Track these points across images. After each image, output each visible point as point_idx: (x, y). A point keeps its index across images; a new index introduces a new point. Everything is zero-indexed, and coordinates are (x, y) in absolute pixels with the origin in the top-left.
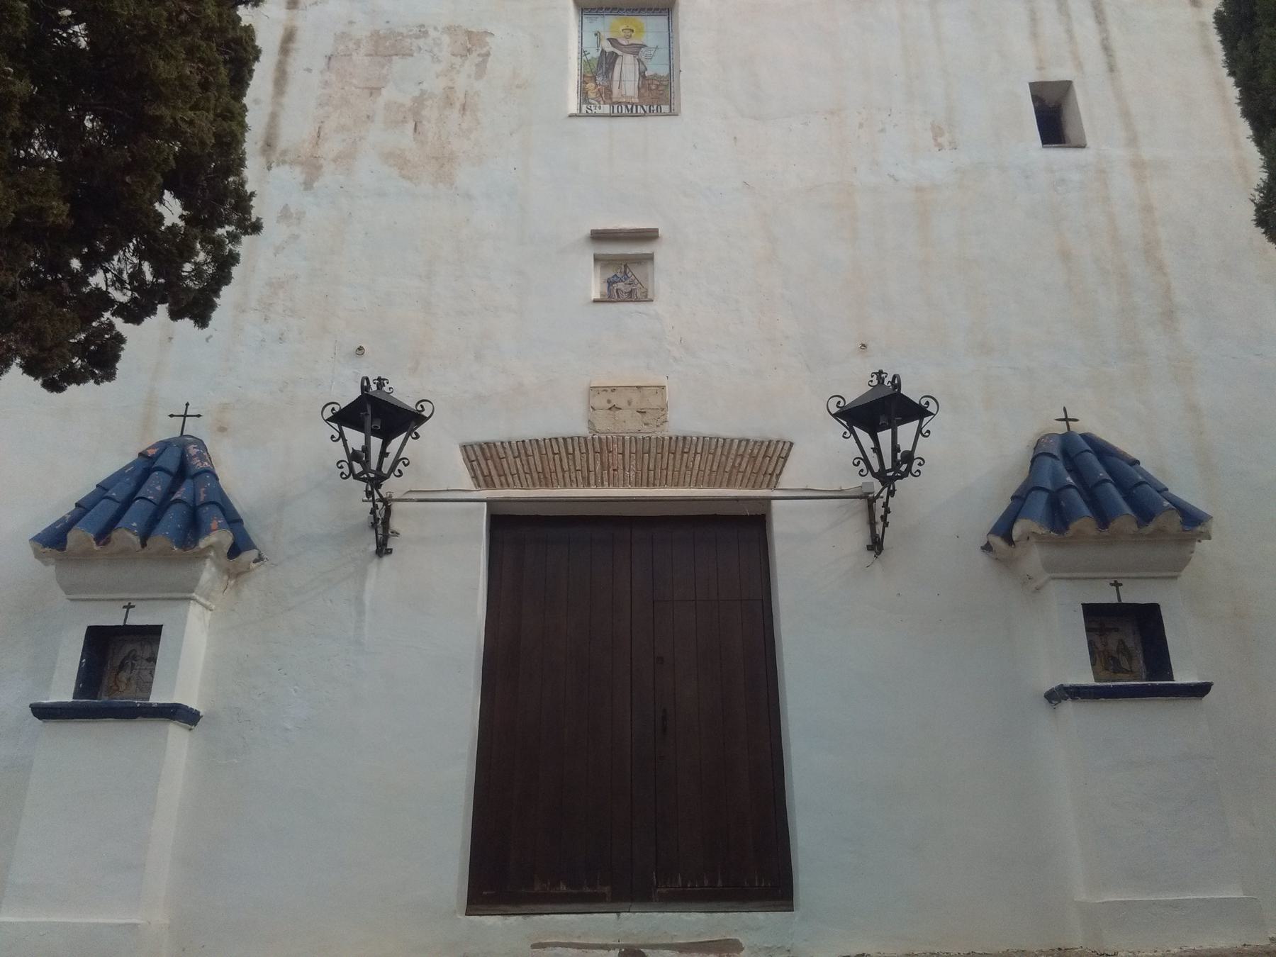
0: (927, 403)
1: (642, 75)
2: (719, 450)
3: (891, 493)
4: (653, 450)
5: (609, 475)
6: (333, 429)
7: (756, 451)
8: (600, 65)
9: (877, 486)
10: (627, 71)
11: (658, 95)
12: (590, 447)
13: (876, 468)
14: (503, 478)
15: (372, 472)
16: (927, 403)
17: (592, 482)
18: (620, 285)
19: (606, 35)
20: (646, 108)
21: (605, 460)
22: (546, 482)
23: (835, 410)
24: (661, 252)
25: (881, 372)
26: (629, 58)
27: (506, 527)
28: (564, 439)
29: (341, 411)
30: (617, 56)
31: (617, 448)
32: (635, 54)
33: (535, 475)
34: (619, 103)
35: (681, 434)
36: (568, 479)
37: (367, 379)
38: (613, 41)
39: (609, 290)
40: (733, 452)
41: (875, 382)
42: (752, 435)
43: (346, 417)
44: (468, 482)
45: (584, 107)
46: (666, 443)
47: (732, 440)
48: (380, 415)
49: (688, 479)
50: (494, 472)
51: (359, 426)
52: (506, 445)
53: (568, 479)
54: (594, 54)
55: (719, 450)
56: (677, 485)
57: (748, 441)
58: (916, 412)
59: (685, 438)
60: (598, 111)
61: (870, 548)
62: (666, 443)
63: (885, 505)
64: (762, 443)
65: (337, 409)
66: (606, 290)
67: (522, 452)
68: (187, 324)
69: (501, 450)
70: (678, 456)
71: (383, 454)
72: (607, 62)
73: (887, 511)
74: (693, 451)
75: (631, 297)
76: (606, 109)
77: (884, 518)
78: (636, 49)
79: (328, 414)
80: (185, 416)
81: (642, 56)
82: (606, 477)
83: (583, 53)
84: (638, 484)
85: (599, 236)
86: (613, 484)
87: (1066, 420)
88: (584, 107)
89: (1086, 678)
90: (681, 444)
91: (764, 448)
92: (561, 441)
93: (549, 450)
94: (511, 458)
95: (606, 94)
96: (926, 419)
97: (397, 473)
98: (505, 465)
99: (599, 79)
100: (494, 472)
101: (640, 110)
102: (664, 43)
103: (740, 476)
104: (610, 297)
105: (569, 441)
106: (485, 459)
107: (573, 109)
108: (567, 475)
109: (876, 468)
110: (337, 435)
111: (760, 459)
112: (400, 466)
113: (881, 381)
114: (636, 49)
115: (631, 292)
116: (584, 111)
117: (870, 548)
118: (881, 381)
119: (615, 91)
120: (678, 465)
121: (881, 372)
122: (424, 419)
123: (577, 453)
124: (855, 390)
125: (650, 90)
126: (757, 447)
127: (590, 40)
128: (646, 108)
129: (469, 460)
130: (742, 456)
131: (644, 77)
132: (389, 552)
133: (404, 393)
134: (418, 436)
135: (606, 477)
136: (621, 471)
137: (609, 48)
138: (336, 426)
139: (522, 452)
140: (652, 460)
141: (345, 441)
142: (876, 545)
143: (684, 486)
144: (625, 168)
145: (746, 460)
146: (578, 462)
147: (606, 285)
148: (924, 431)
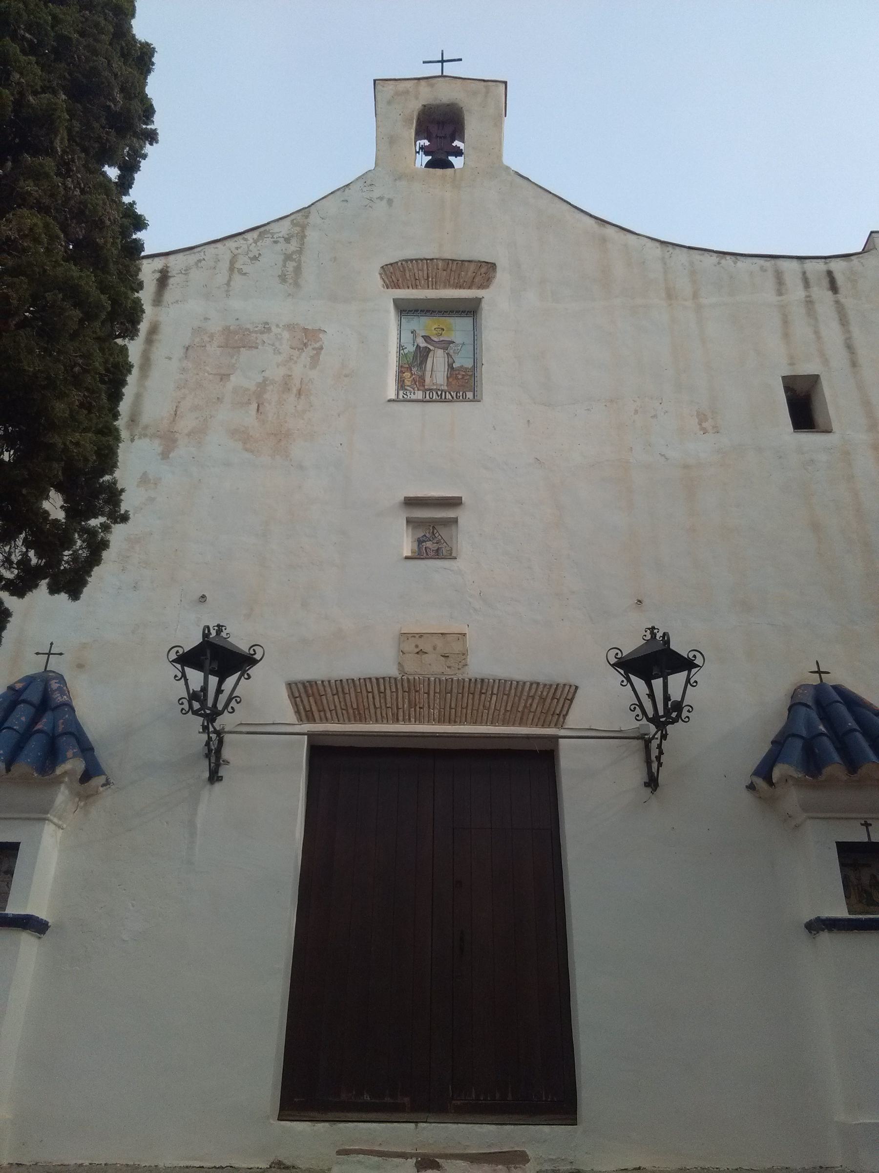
0: (695, 656)
1: (451, 366)
2: (513, 691)
3: (664, 737)
4: (455, 691)
7: (545, 694)
10: (437, 364)
11: (464, 384)
12: (399, 686)
13: (650, 714)
16: (695, 656)
17: (401, 718)
20: (454, 394)
23: (613, 661)
25: (653, 628)
26: (440, 352)
27: (328, 761)
28: (377, 679)
30: (430, 350)
31: (423, 688)
32: (445, 349)
33: (351, 711)
34: (431, 390)
35: (479, 676)
38: (426, 338)
41: (649, 637)
46: (467, 684)
47: (525, 683)
48: (217, 657)
49: (485, 718)
51: (198, 666)
52: (326, 683)
54: (411, 348)
55: (513, 691)
56: (475, 723)
57: (538, 684)
58: (686, 664)
59: (482, 680)
60: (413, 397)
61: (647, 785)
62: (467, 684)
63: (659, 746)
64: (551, 686)
67: (340, 690)
69: (321, 688)
70: (477, 697)
71: (219, 691)
72: (422, 355)
73: (661, 753)
75: (438, 555)
76: (419, 395)
77: (658, 758)
78: (446, 345)
79: (173, 656)
80: (49, 654)
82: (413, 713)
83: (401, 347)
84: (441, 721)
85: (411, 502)
86: (419, 720)
87: (819, 672)
88: (401, 393)
92: (374, 681)
93: (364, 688)
95: (420, 383)
96: (694, 671)
97: (230, 709)
98: (325, 702)
99: (414, 370)
100: (314, 708)
101: (448, 396)
104: (420, 554)
105: (381, 681)
106: (307, 696)
109: (650, 714)
111: (549, 700)
112: (233, 703)
113: (653, 635)
117: (647, 785)
119: (428, 380)
121: (653, 628)
123: (388, 692)
125: (457, 378)
127: (407, 337)
128: (454, 394)
129: (293, 697)
130: (533, 698)
131: (452, 368)
133: (239, 638)
134: (249, 677)
135: (413, 713)
136: (426, 709)
137: (423, 344)
138: (179, 666)
139: (340, 690)
141: (186, 680)
144: (436, 446)
147: (416, 544)
148: (692, 681)
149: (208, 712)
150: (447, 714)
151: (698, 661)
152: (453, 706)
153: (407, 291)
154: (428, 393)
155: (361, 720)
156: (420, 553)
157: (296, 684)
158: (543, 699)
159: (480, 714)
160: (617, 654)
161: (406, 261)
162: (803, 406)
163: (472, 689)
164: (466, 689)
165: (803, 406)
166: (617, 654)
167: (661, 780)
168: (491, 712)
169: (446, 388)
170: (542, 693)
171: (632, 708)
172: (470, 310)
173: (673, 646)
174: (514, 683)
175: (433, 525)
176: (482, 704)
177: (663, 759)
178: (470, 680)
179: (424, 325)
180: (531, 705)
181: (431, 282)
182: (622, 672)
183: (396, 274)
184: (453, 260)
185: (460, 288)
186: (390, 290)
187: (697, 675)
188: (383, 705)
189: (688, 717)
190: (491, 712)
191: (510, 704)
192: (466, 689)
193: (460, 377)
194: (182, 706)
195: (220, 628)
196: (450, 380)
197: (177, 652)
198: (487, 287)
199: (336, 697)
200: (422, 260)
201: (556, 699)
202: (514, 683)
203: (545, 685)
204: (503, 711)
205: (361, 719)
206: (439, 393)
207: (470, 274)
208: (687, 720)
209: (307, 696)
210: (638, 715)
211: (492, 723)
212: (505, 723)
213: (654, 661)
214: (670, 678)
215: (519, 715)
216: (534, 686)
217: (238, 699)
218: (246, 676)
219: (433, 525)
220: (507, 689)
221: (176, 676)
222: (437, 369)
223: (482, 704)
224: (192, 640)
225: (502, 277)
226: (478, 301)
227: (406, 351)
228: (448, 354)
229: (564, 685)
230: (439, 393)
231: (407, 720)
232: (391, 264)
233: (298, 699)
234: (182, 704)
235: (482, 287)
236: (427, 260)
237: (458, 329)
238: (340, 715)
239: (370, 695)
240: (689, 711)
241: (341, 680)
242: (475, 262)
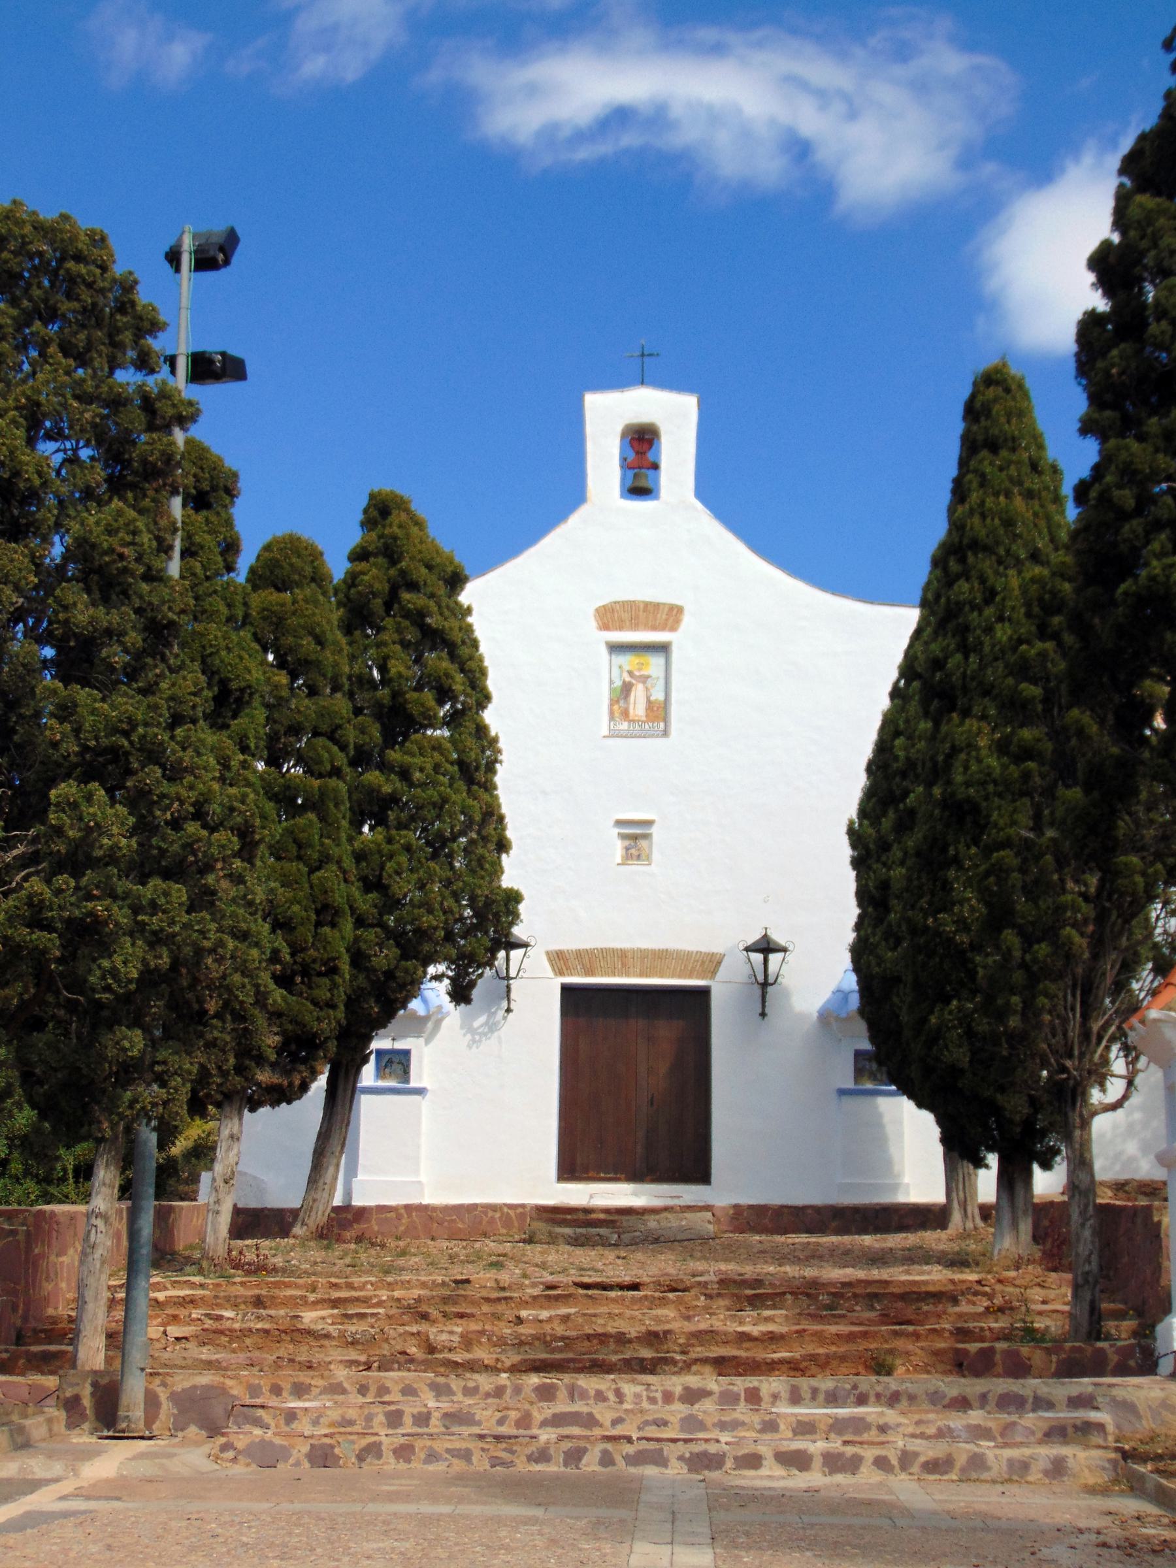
5: (626, 971)
10: (638, 697)
18: (633, 851)
19: (626, 668)
22: (590, 972)
24: (654, 830)
26: (640, 687)
27: (576, 1000)
32: (644, 683)
38: (630, 673)
42: (703, 949)
44: (550, 973)
54: (618, 683)
56: (662, 977)
72: (627, 689)
83: (611, 682)
84: (641, 975)
85: (620, 823)
86: (628, 975)
89: (850, 1084)
95: (625, 714)
102: (662, 675)
106: (559, 960)
107: (606, 733)
114: (645, 679)
119: (631, 711)
124: (753, 937)
127: (616, 672)
129: (550, 960)
137: (628, 679)
142: (763, 1014)
175: (635, 838)
179: (628, 661)
181: (635, 626)
183: (609, 616)
201: (711, 964)
209: (559, 960)
212: (680, 977)
213: (766, 947)
219: (635, 837)
222: (638, 704)
231: (620, 975)
235: (673, 629)
237: (654, 665)
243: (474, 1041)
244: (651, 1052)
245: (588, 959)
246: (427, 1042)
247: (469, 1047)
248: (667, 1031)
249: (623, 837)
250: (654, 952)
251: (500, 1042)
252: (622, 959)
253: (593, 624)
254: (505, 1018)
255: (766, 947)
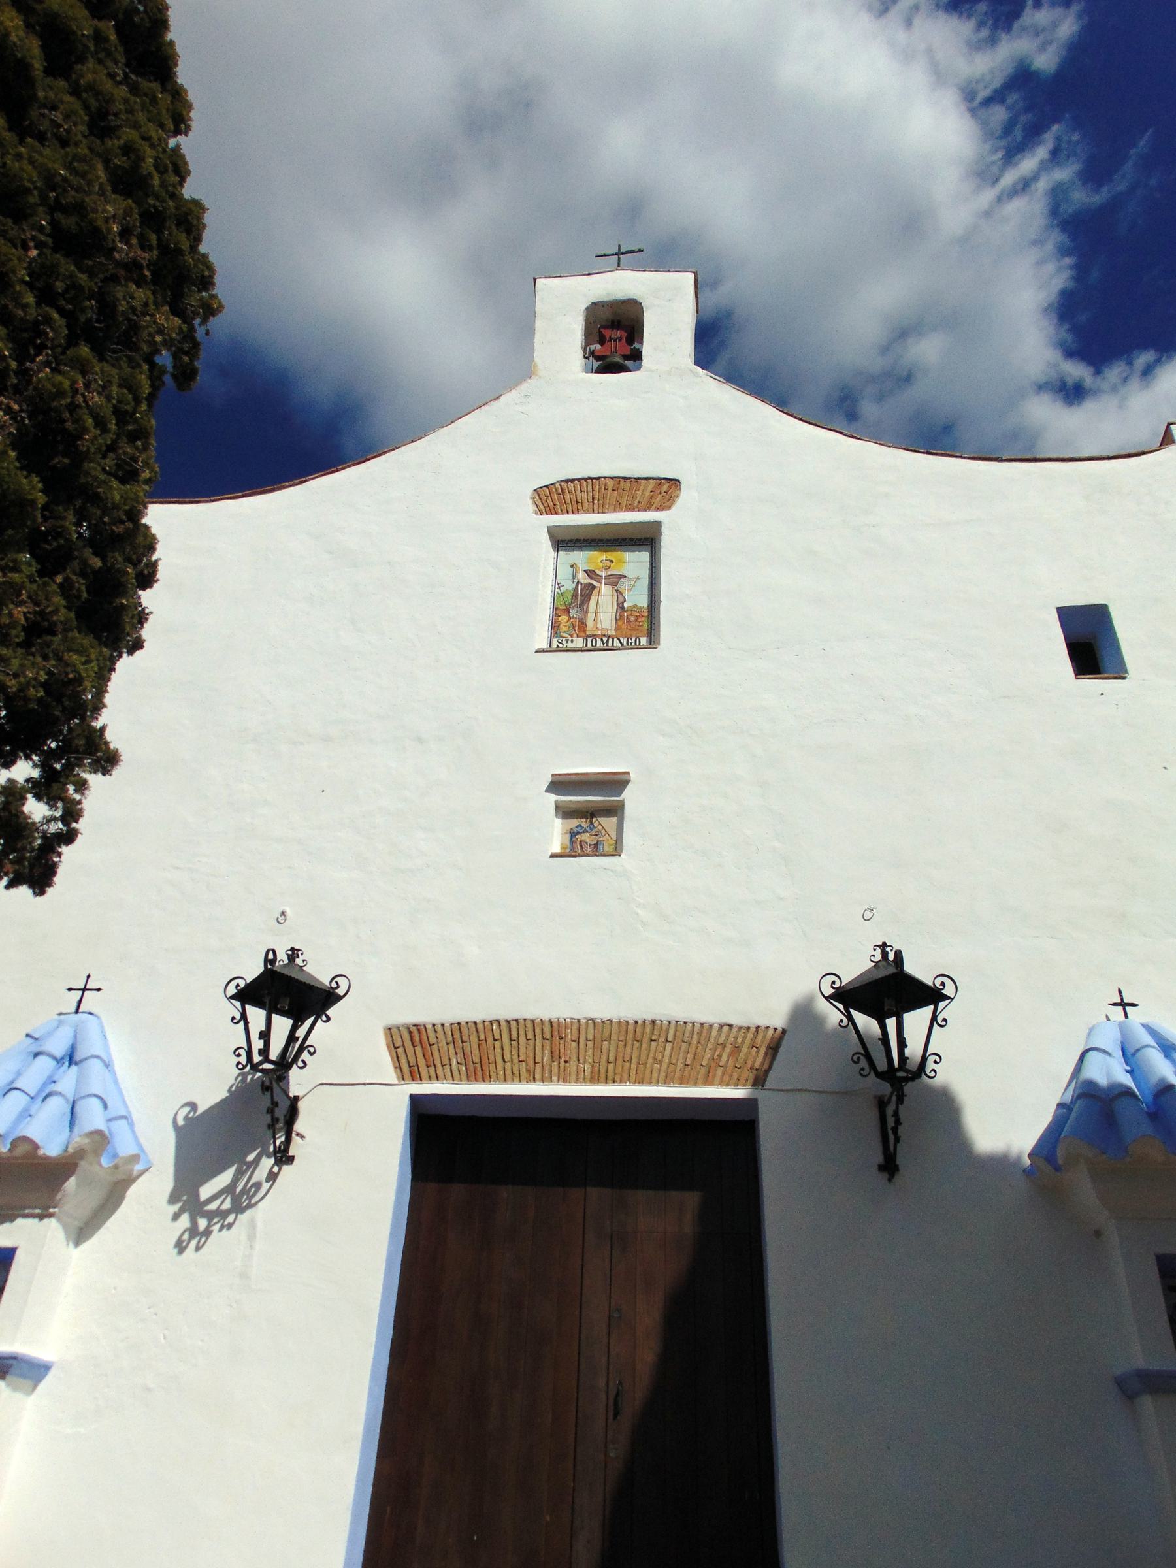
0: (943, 984)
1: (620, 606)
2: (695, 1037)
3: (901, 1099)
4: (614, 1037)
6: (234, 1008)
7: (739, 1040)
8: (575, 596)
9: (886, 1088)
11: (642, 626)
12: (538, 1031)
13: (882, 1065)
14: (432, 1069)
15: (272, 1062)
16: (943, 984)
17: (538, 1076)
18: (586, 837)
19: (582, 567)
20: (624, 641)
21: (555, 1049)
23: (828, 991)
25: (884, 945)
26: (605, 590)
27: (444, 1142)
28: (508, 1022)
29: (248, 986)
30: (594, 587)
31: (570, 1034)
32: (613, 585)
33: (471, 1067)
34: (593, 636)
35: (649, 1017)
36: (508, 1072)
37: (274, 952)
38: (590, 573)
39: (572, 842)
40: (712, 1040)
41: (878, 957)
42: (735, 1021)
43: (247, 995)
45: (555, 641)
46: (631, 1028)
47: (711, 1026)
48: (287, 992)
49: (655, 1075)
50: (422, 1062)
51: (259, 1004)
52: (439, 1028)
53: (508, 1072)
54: (569, 586)
55: (695, 1037)
56: (641, 1082)
57: (731, 1026)
58: (931, 996)
59: (653, 1022)
60: (570, 645)
61: (881, 1168)
62: (631, 1028)
63: (896, 1114)
64: (749, 1028)
65: (242, 984)
66: (568, 843)
67: (457, 1036)
68: (24, 891)
69: (431, 1034)
70: (645, 1045)
71: (292, 1038)
72: (584, 595)
73: (898, 1122)
74: (663, 1039)
75: (596, 850)
76: (579, 643)
77: (895, 1130)
78: (615, 580)
79: (232, 990)
80: (84, 990)
81: (620, 587)
82: (555, 1070)
84: (594, 1079)
85: (559, 785)
86: (564, 1079)
87: (1123, 1004)
88: (555, 641)
90: (648, 1030)
91: (750, 1035)
92: (503, 1024)
93: (489, 1035)
94: (443, 1044)
95: (580, 627)
96: (942, 1005)
97: (300, 1064)
98: (436, 1054)
99: (573, 613)
100: (422, 1062)
101: (617, 644)
102: (645, 573)
103: (720, 1070)
104: (574, 849)
105: (514, 1024)
106: (413, 1046)
108: (508, 1066)
109: (882, 1065)
110: (238, 1016)
111: (745, 1049)
112: (305, 1056)
113: (885, 955)
115: (597, 844)
116: (589, 645)
117: (881, 1168)
118: (885, 955)
119: (590, 623)
120: (643, 1057)
121: (884, 945)
122: (340, 998)
123: (522, 1039)
124: (855, 966)
125: (629, 621)
126: (741, 1034)
127: (565, 573)
128: (624, 641)
129: (393, 1047)
130: (723, 1046)
131: (623, 608)
132: (291, 1160)
133: (319, 969)
134: (328, 1019)
135: (555, 1070)
136: (573, 1063)
138: (238, 1004)
139: (457, 1036)
140: (613, 1049)
141: (246, 1024)
142: (889, 1167)
143: (650, 1082)
144: (602, 708)
145: (727, 1050)
146: (522, 1049)
147: (569, 836)
148: (939, 1019)
149: (271, 1066)
150: (603, 1071)
151: (949, 990)
152: (611, 1059)
153: (566, 516)
154: (590, 640)
155: (565, 1081)
156: (572, 849)
157: (398, 1028)
158: (737, 1048)
159: (648, 1071)
160: (833, 982)
161: (567, 481)
162: (1090, 645)
163: (639, 1035)
164: (631, 1035)
165: (1090, 645)
166: (833, 982)
167: (900, 1161)
168: (664, 1065)
169: (613, 633)
170: (736, 1038)
171: (855, 1058)
172: (646, 539)
173: (910, 968)
174: (697, 1026)
175: (590, 813)
176: (651, 1055)
177: (901, 1129)
178: (636, 1022)
179: (581, 558)
180: (720, 1056)
181: (597, 506)
182: (841, 1007)
184: (625, 478)
185: (633, 510)
186: (545, 517)
187: (947, 1010)
188: (515, 1057)
189: (934, 1070)
190: (664, 1065)
191: (690, 1056)
192: (631, 1035)
193: (632, 619)
194: (239, 1059)
195: (294, 953)
196: (620, 623)
197: (238, 985)
198: (669, 508)
199: (451, 1046)
200: (585, 479)
202: (697, 1026)
203: (740, 1028)
204: (680, 1065)
205: (485, 1078)
206: (605, 639)
207: (648, 494)
208: (933, 1074)
209: (413, 1046)
210: (863, 1069)
211: (667, 1081)
212: (683, 1082)
213: (891, 990)
214: (908, 1017)
215: (703, 1070)
216: (726, 1029)
217: (312, 1050)
218: (324, 1018)
220: (687, 1034)
221: (233, 1018)
222: (603, 611)
223: (651, 1055)
224: (253, 970)
225: (685, 497)
226: (657, 525)
227: (563, 589)
228: (617, 591)
229: (721, 1026)
230: (605, 639)
231: (547, 1079)
232: (547, 486)
233: (400, 1050)
234: (239, 1055)
236: (592, 479)
237: (634, 563)
238: (456, 1073)
239: (498, 1044)
240: (935, 1062)
241: (459, 1024)
242: (654, 479)
243: (193, 1231)
244: (624, 1271)
245: (476, 1044)
246: (81, 1233)
247: (180, 1247)
248: (664, 1222)
249: (565, 812)
250: (623, 1025)
251: (251, 1237)
252: (552, 1040)
253: (531, 507)
254: (272, 1177)
255: (891, 990)
